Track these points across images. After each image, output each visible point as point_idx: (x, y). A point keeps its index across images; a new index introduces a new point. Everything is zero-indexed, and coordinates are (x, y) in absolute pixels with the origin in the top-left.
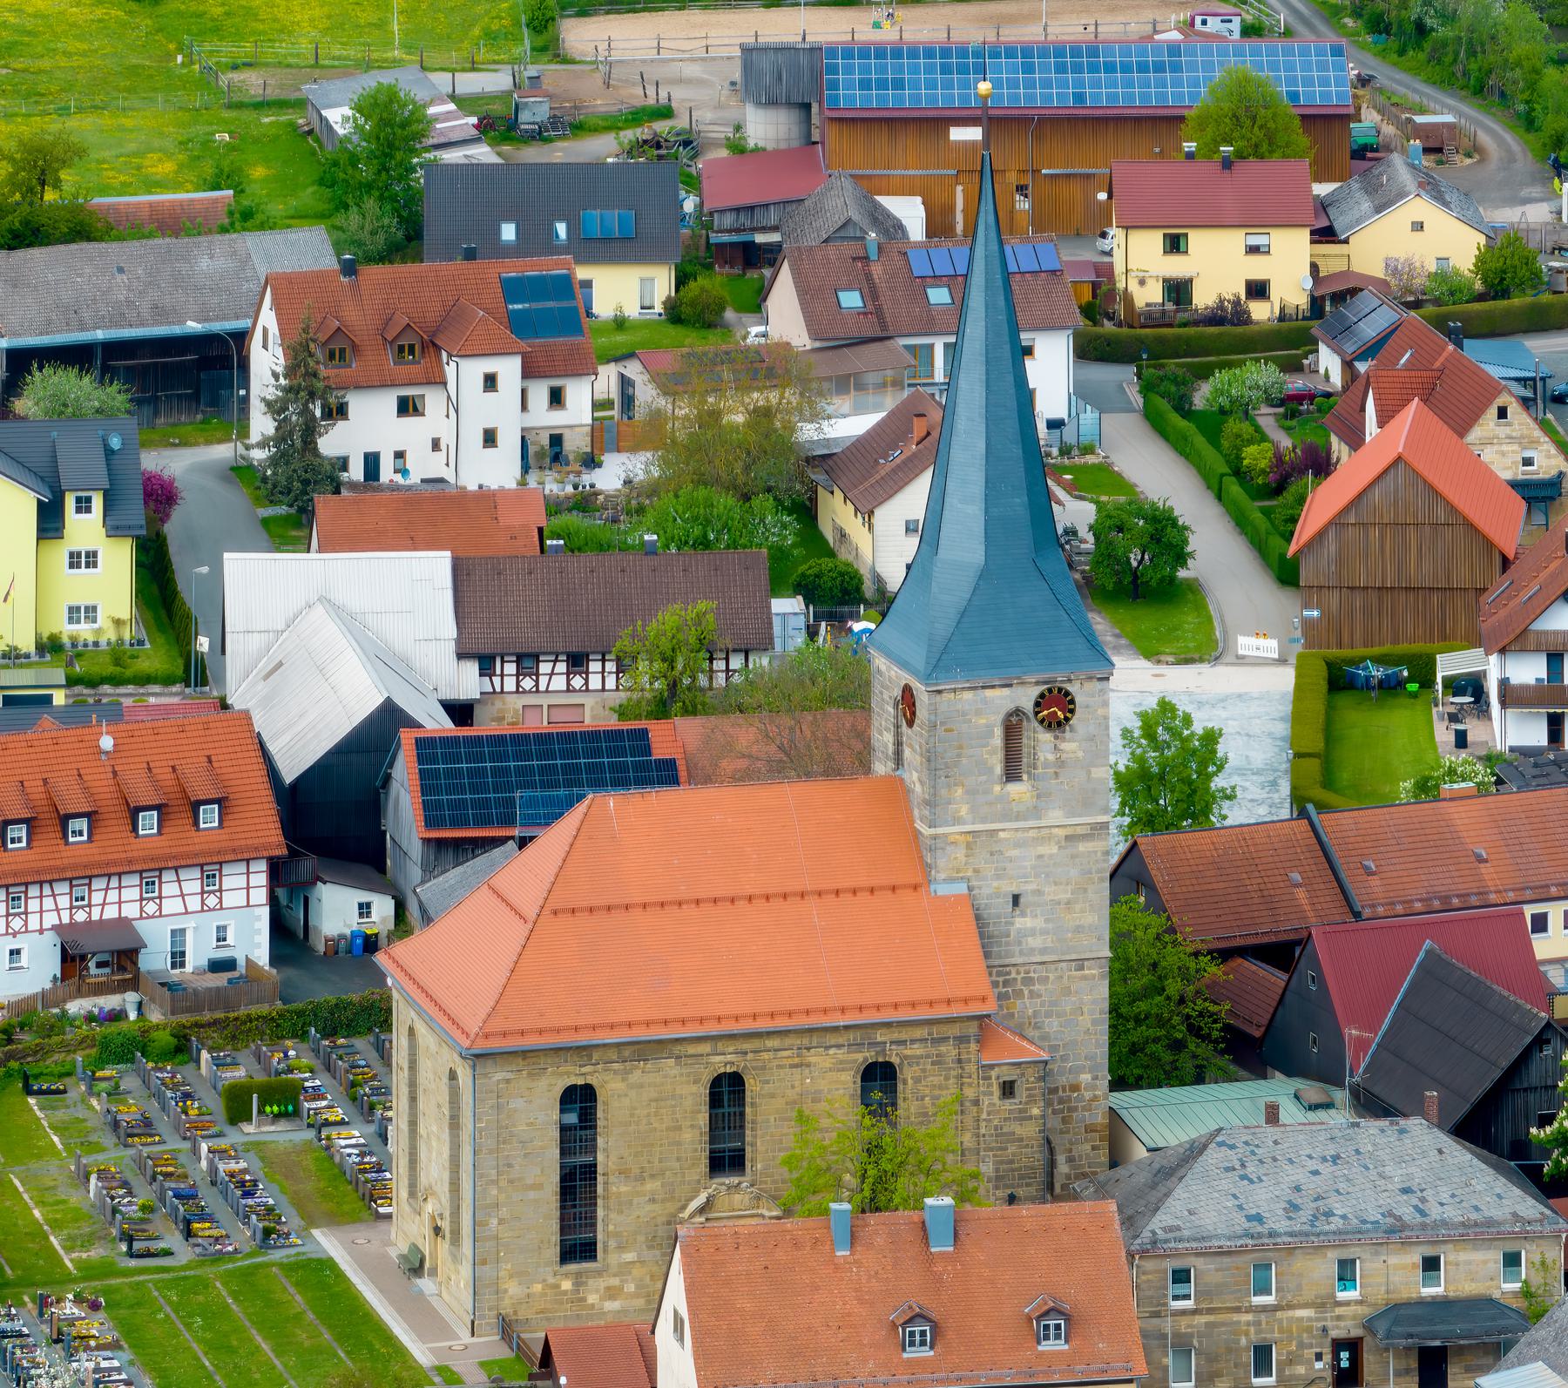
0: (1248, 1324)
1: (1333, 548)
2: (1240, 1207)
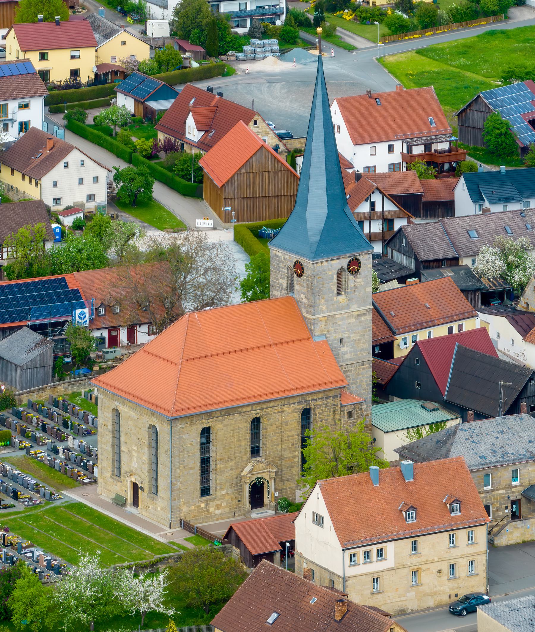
0: (483, 498)
1: (236, 183)
2: (476, 453)
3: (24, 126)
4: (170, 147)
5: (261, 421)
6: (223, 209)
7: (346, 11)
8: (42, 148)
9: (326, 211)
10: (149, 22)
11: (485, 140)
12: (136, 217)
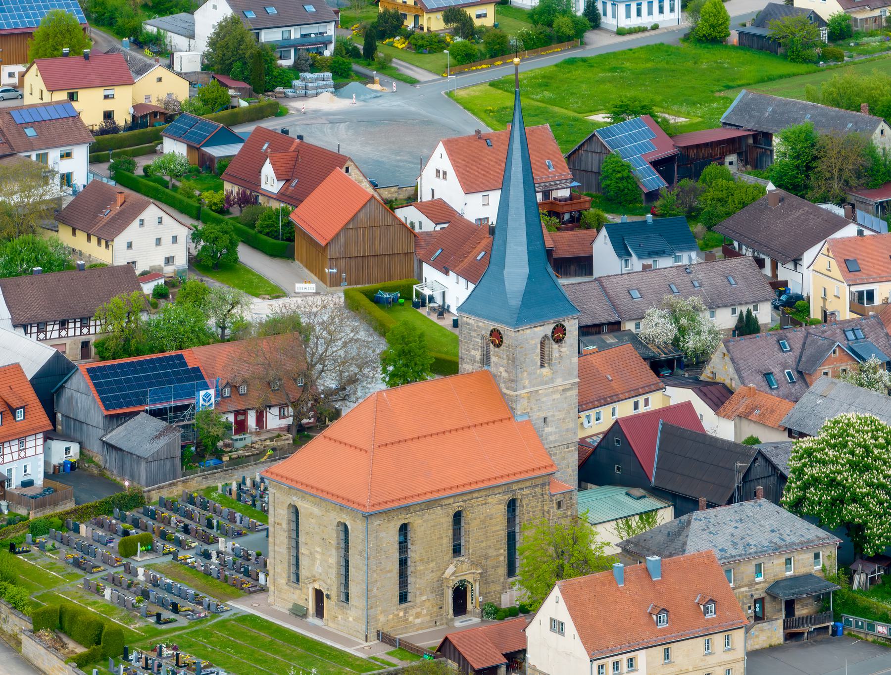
1: (342, 240)
3: (67, 179)
4: (245, 200)
5: (464, 514)
6: (327, 271)
7: (398, 38)
8: (110, 204)
9: (526, 271)
10: (176, 55)
11: (603, 186)
12: (222, 282)
